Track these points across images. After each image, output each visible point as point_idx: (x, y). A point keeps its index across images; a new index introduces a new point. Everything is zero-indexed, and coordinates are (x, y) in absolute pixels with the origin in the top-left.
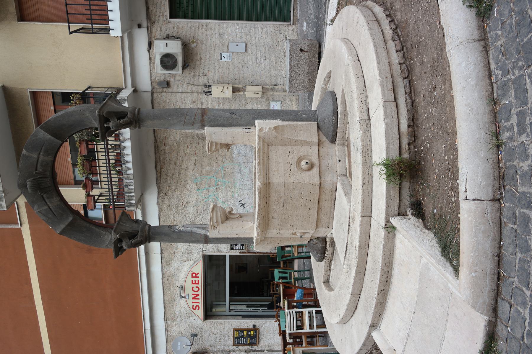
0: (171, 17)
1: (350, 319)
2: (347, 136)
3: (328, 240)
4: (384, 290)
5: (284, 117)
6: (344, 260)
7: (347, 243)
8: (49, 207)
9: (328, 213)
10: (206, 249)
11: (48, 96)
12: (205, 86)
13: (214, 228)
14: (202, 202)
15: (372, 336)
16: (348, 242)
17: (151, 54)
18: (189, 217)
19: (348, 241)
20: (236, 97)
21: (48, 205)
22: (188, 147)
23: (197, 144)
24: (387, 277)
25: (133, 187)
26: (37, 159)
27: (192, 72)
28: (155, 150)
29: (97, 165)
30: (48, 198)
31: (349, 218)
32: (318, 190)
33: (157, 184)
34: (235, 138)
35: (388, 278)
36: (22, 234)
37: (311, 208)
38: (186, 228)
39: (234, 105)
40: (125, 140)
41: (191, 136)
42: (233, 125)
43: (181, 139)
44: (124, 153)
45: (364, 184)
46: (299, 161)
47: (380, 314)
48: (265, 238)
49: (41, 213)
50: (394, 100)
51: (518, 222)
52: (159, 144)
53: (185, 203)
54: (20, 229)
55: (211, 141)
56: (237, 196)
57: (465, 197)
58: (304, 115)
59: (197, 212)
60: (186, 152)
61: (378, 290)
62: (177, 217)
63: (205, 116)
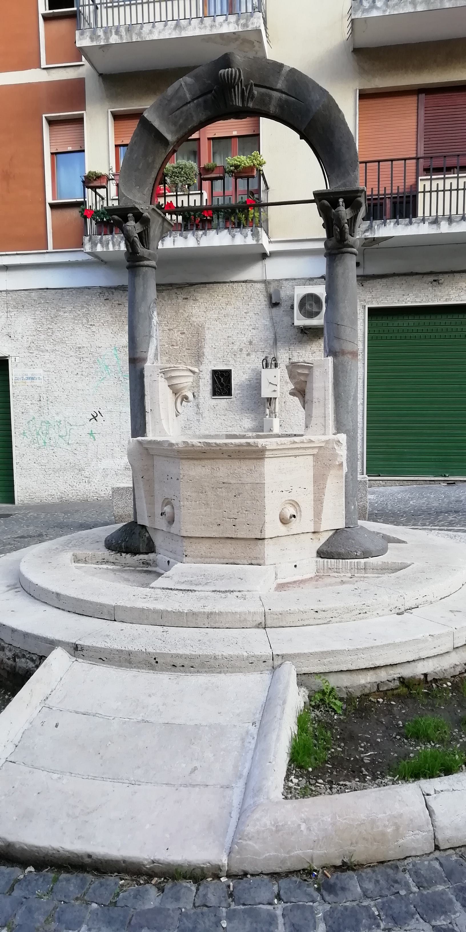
0: (370, 309)
1: (50, 605)
2: (331, 574)
3: (151, 556)
4: (157, 662)
5: (351, 477)
6: (161, 588)
7: (195, 591)
8: (189, 102)
9: (212, 555)
10: (17, 361)
11: (55, 147)
12: (275, 359)
13: (161, 373)
14: (97, 355)
15: (53, 649)
16: (197, 592)
17: (319, 280)
18: (71, 335)
19: (199, 591)
20: (259, 404)
21: (193, 100)
22: (183, 333)
23: (187, 347)
24: (183, 666)
25: (111, 248)
26: (274, 88)
27: (294, 340)
28: (176, 284)
29: (178, 193)
30: (205, 102)
31: (239, 591)
32: (254, 537)
33: (123, 285)
34: (317, 403)
35: (182, 668)
36: (30, 69)
37: (221, 527)
38: (155, 328)
39: (248, 401)
40: (197, 239)
41: (199, 338)
42: (338, 400)
43: (195, 324)
44: (176, 237)
45: (317, 612)
46: (295, 504)
47: (104, 659)
48: (153, 455)
49: (179, 89)
50: (455, 646)
51: (428, 893)
52: (185, 290)
53: (94, 328)
54: (39, 67)
55: (312, 367)
56: (109, 408)
57: (428, 792)
58: (353, 507)
59: (80, 348)
60: (176, 330)
61: (156, 653)
62: (70, 317)
63: (350, 357)
